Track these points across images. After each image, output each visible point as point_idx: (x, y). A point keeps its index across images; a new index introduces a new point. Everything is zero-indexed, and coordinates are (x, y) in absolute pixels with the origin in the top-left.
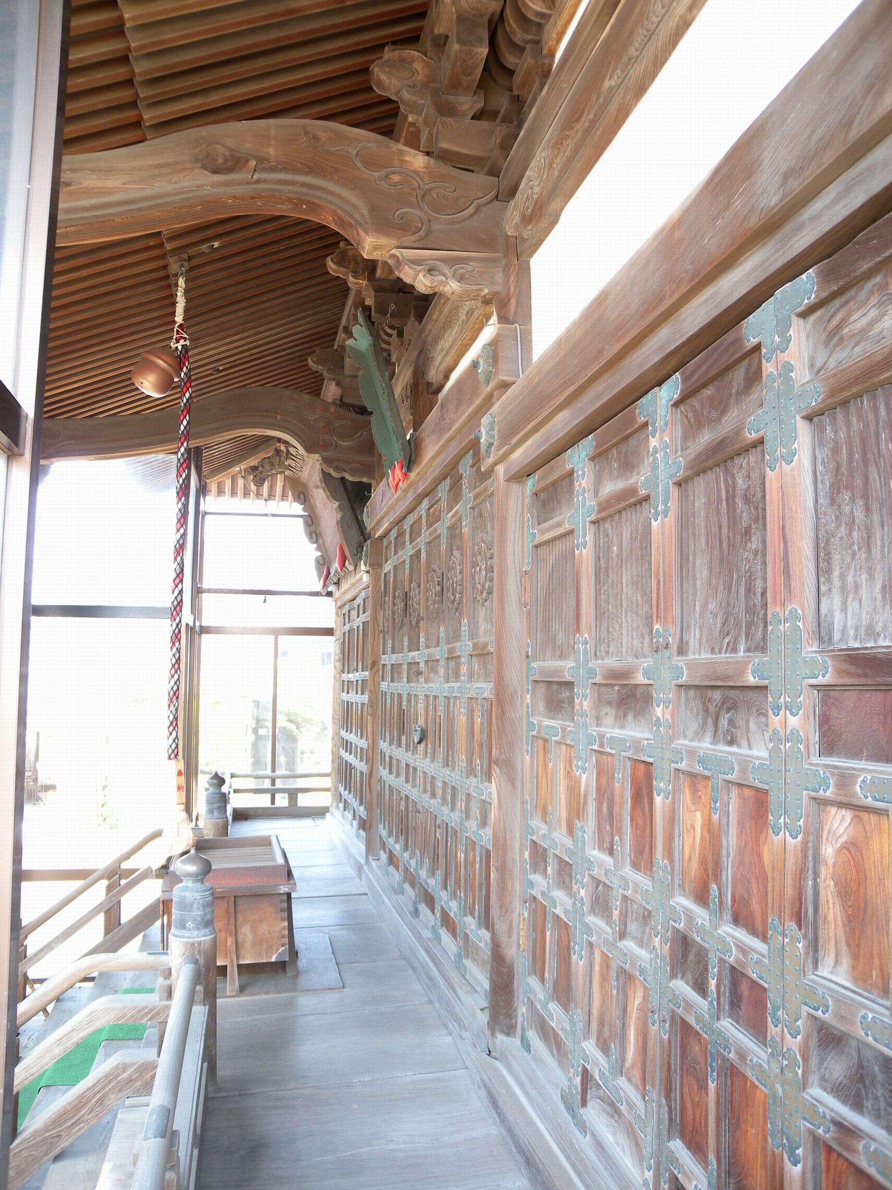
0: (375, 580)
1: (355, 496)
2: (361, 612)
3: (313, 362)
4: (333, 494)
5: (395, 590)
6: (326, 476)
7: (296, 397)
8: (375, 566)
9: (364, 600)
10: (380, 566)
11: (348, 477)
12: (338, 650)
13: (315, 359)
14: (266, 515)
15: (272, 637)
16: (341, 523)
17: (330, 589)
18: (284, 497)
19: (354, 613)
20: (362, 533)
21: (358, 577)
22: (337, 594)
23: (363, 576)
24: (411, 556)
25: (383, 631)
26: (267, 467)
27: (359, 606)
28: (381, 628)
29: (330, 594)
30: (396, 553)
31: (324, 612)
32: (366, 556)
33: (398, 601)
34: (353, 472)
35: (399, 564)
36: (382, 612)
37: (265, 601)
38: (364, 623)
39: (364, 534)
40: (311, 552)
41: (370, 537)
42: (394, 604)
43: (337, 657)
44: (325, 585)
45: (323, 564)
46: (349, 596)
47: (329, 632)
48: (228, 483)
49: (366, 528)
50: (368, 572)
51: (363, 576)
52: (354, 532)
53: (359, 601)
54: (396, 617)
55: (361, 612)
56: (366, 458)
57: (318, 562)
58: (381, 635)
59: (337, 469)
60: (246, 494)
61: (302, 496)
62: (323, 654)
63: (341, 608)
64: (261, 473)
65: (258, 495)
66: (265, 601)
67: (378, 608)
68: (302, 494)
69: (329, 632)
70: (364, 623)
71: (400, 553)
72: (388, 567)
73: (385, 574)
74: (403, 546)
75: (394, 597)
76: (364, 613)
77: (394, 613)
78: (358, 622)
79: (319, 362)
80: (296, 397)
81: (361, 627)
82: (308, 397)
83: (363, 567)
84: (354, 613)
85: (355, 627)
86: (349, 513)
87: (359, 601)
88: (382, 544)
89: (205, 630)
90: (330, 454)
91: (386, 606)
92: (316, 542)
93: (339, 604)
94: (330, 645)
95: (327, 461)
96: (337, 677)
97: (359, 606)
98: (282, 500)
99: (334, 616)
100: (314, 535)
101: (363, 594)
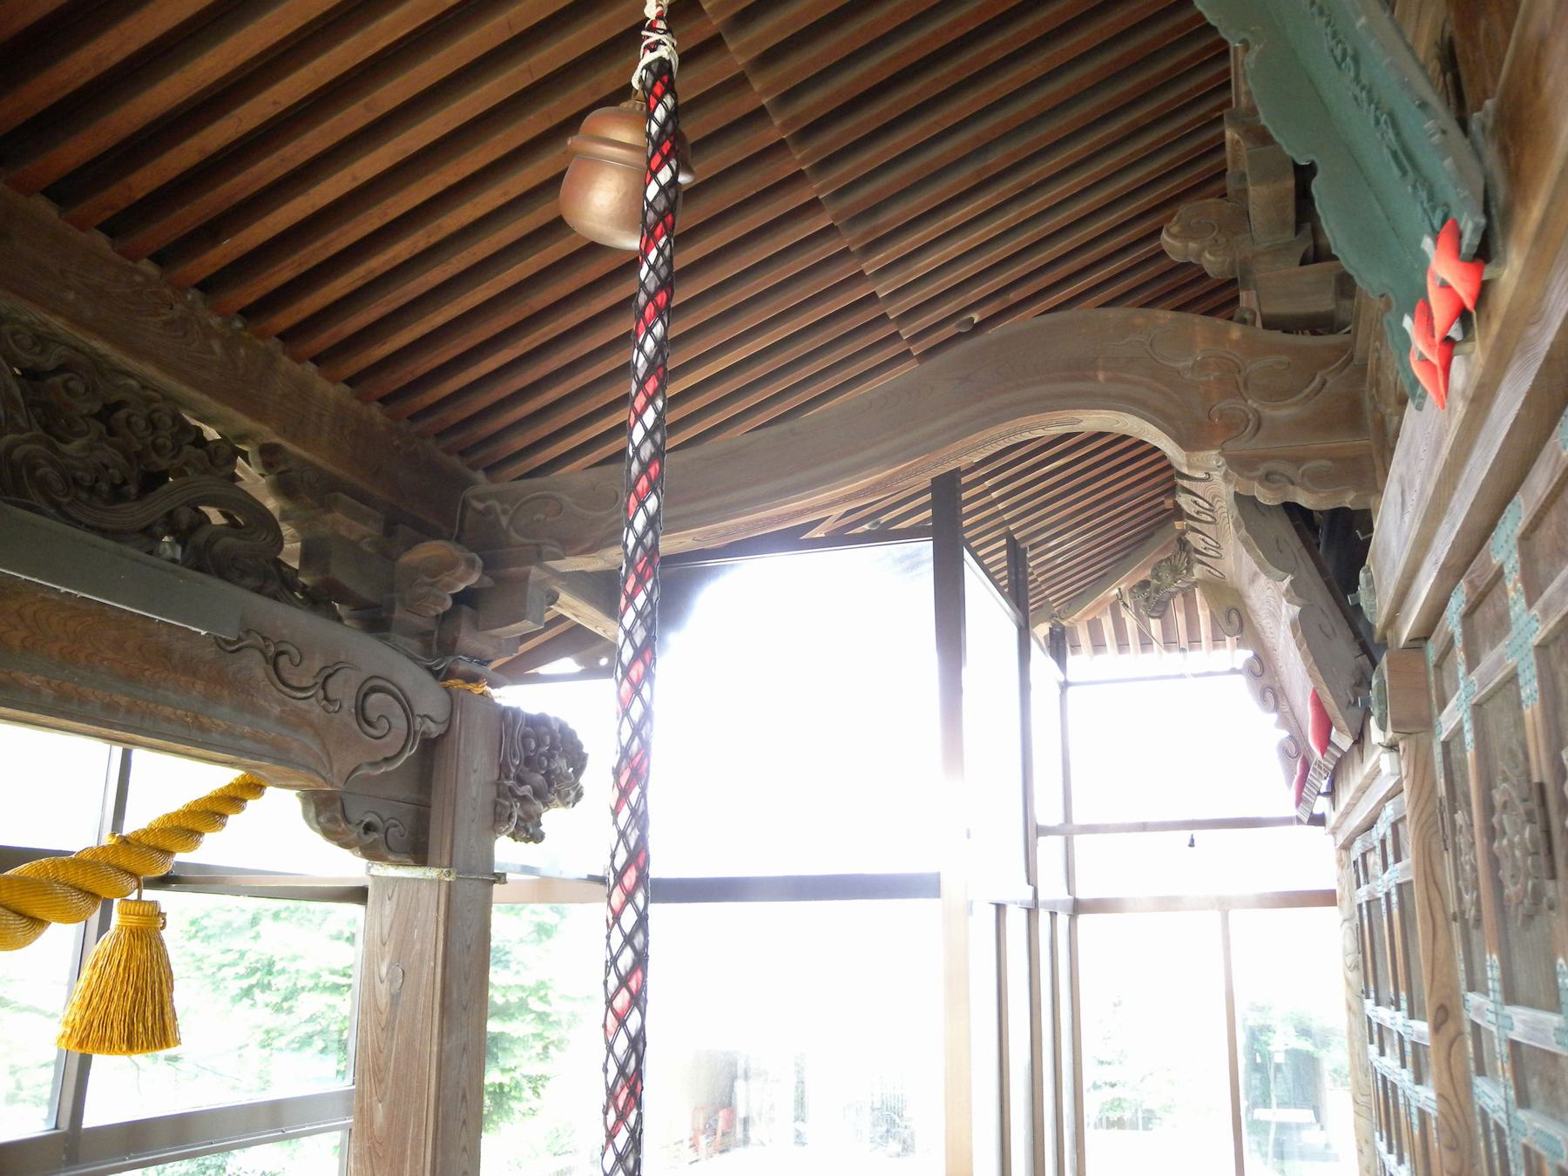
0: (1421, 766)
1: (1332, 546)
2: (1391, 859)
3: (1174, 236)
4: (1273, 558)
5: (1487, 786)
6: (1245, 502)
7: (1138, 321)
8: (1414, 725)
9: (1394, 826)
10: (1428, 725)
11: (1305, 500)
12: (1350, 944)
13: (1175, 229)
14: (1181, 676)
15: (1216, 915)
16: (1305, 628)
17: (1317, 811)
18: (1217, 640)
19: (1374, 860)
20: (1365, 649)
21: (1368, 766)
22: (1332, 818)
23: (1383, 764)
24: (1542, 647)
25: (1460, 916)
26: (1166, 576)
27: (1383, 842)
28: (1453, 908)
29: (1318, 820)
30: (1472, 662)
31: (1315, 858)
32: (1382, 702)
33: (1504, 820)
34: (1317, 480)
35: (1489, 697)
36: (1448, 858)
37: (1192, 844)
38: (1400, 887)
39: (1367, 644)
40: (1268, 731)
41: (1384, 645)
42: (1491, 833)
43: (1349, 960)
44: (1300, 800)
45: (1298, 760)
46: (1356, 820)
47: (1327, 898)
48: (1107, 623)
49: (1370, 626)
50: (1392, 747)
51: (1383, 764)
52: (1345, 651)
53: (1382, 828)
54: (1505, 873)
55: (1391, 859)
56: (1343, 443)
57: (1284, 752)
58: (1456, 927)
59: (1267, 478)
60: (1146, 642)
61: (1234, 617)
62: (1360, 906)
63: (1347, 847)
64: (1157, 591)
65: (1169, 642)
66: (1192, 844)
67: (1437, 846)
68: (1235, 618)
69: (1327, 898)
70: (1400, 887)
71: (1488, 659)
72: (1453, 716)
73: (1446, 745)
74: (1502, 624)
75: (1489, 808)
76: (1398, 859)
77: (1494, 862)
78: (1385, 881)
79: (1188, 233)
80: (1138, 321)
81: (1394, 899)
82: (1170, 315)
83: (1376, 735)
84: (1374, 860)
85: (1381, 895)
86: (1321, 597)
87: (1382, 828)
88: (1425, 661)
89: (1078, 907)
90: (1245, 445)
91: (1462, 840)
92: (1276, 708)
93: (1341, 839)
94: (1330, 932)
95: (1239, 464)
96: (1355, 1006)
97: (1383, 842)
98: (1215, 647)
99: (1335, 867)
100: (1269, 695)
101: (1389, 812)
